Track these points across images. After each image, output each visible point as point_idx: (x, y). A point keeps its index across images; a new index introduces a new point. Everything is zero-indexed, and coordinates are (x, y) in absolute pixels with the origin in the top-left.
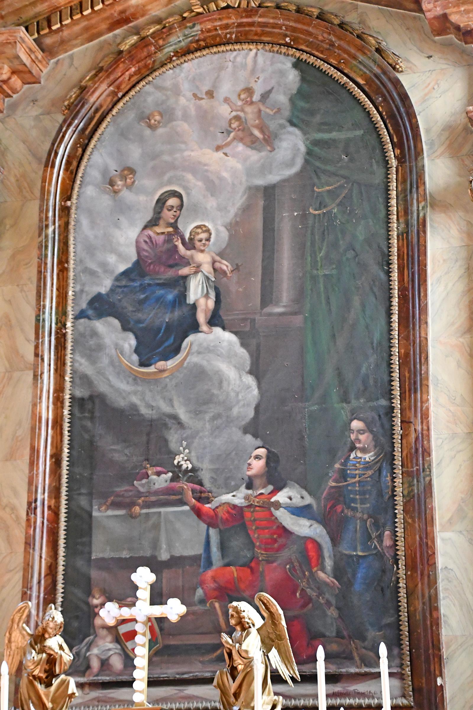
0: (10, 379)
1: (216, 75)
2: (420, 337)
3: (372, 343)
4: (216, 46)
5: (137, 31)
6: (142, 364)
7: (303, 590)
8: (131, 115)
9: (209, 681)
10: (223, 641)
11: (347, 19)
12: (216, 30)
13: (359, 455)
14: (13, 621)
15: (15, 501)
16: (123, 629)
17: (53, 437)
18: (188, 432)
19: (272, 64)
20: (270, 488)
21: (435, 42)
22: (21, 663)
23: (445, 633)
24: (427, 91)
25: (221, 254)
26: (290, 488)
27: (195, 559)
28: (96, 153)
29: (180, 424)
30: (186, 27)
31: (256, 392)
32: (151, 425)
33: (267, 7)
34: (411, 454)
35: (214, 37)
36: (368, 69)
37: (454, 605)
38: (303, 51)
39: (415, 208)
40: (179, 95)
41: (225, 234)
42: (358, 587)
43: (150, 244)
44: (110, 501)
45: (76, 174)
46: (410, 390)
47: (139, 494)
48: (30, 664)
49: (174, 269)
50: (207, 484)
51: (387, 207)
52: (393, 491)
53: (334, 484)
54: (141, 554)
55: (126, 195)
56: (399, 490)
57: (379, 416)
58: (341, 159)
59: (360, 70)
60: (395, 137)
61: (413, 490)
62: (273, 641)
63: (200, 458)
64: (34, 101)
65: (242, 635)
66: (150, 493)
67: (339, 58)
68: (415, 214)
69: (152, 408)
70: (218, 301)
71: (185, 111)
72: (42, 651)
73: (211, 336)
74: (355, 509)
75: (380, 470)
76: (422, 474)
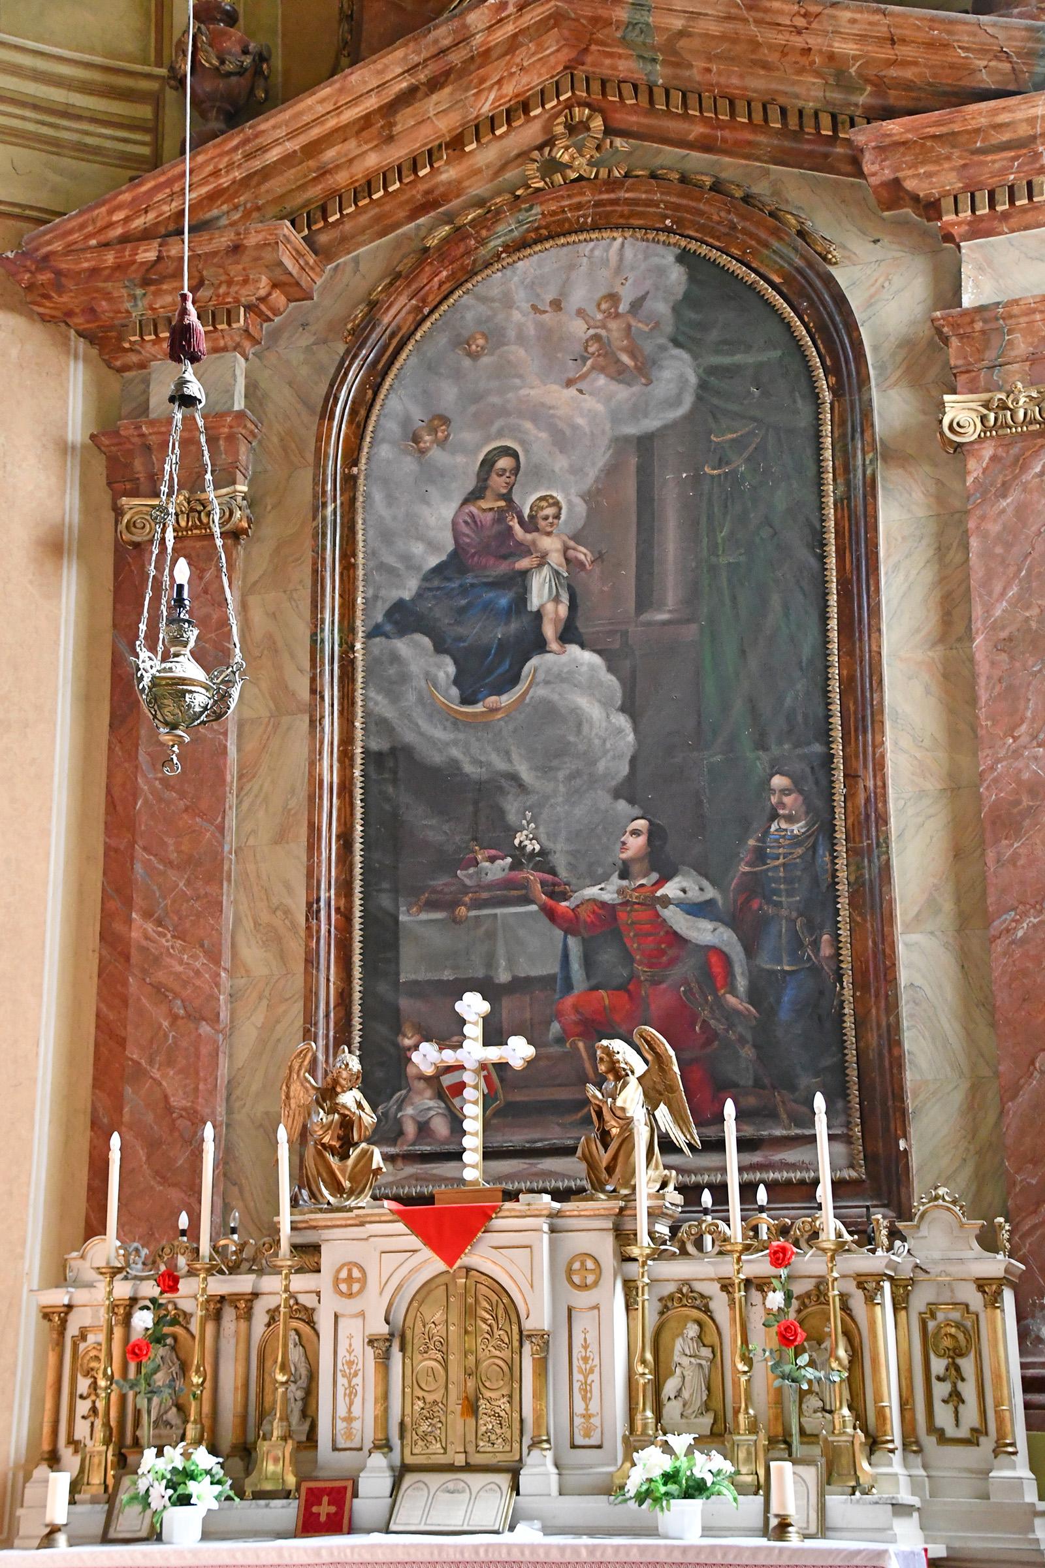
0: (276, 727)
1: (564, 277)
2: (870, 651)
3: (801, 662)
4: (564, 235)
5: (449, 218)
6: (466, 701)
7: (704, 1021)
8: (443, 340)
9: (570, 1151)
10: (589, 1095)
11: (755, 190)
12: (564, 211)
13: (784, 826)
14: (291, 1068)
15: (288, 901)
16: (447, 1080)
17: (339, 810)
18: (532, 799)
19: (646, 258)
20: (655, 876)
21: (883, 219)
22: (305, 1127)
23: (910, 1077)
24: (873, 290)
25: (576, 538)
26: (683, 876)
27: (547, 981)
28: (392, 396)
29: (521, 786)
30: (520, 210)
31: (631, 737)
32: (480, 790)
33: (637, 176)
34: (859, 823)
35: (560, 223)
36: (786, 261)
37: (924, 1037)
38: (691, 238)
39: (859, 462)
40: (511, 307)
41: (581, 508)
42: (784, 1014)
43: (472, 525)
44: (423, 898)
45: (365, 427)
46: (856, 730)
47: (465, 890)
48: (317, 1129)
49: (508, 562)
50: (563, 873)
51: (819, 461)
52: (834, 876)
53: (747, 869)
54: (470, 974)
55: (437, 455)
56: (842, 875)
57: (812, 768)
58: (749, 393)
59: (776, 262)
60: (828, 360)
61: (862, 875)
62: (661, 1094)
63: (552, 836)
64: (304, 325)
65: (616, 1086)
66: (481, 887)
67: (743, 247)
68: (860, 471)
69: (480, 764)
70: (573, 607)
71: (520, 328)
72: (332, 1110)
73: (564, 658)
74: (778, 905)
75: (814, 848)
76: (876, 852)
